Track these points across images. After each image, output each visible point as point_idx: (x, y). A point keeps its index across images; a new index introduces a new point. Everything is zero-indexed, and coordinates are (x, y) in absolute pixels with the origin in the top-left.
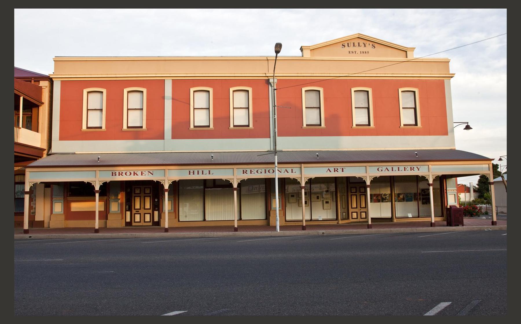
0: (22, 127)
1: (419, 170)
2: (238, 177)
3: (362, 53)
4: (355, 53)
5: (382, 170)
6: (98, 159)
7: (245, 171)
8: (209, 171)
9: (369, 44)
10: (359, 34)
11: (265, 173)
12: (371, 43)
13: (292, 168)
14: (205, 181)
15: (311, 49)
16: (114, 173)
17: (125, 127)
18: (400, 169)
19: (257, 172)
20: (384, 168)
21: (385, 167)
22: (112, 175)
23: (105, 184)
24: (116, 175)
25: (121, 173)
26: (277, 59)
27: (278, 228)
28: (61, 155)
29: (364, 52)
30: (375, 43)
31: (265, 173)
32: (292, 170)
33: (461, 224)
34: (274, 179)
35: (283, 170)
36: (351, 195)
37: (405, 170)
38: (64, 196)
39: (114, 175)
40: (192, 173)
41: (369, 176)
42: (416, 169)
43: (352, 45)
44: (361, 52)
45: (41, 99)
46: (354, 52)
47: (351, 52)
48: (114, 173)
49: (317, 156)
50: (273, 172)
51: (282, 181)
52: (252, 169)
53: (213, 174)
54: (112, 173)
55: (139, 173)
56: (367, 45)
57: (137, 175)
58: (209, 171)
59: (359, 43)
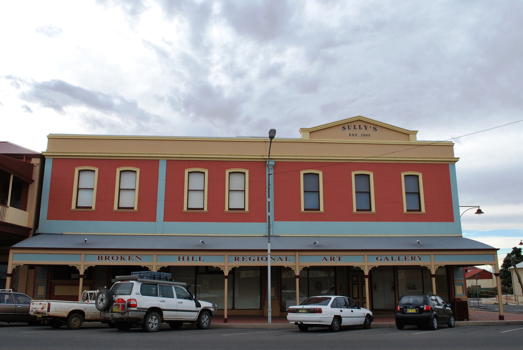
0: (10, 206)
1: (420, 260)
2: (370, 264)
3: (363, 135)
4: (356, 136)
5: (381, 260)
6: (85, 242)
7: (413, 258)
8: (200, 258)
9: (370, 127)
10: (359, 116)
11: (258, 260)
12: (372, 126)
13: (193, 256)
14: (197, 267)
15: (310, 131)
16: (100, 257)
17: (227, 209)
18: (400, 258)
19: (250, 259)
20: (383, 257)
21: (385, 256)
22: (99, 259)
23: (90, 268)
24: (102, 259)
25: (333, 258)
26: (272, 141)
27: (270, 319)
28: (318, 238)
29: (365, 135)
30: (376, 126)
31: (258, 260)
32: (392, 258)
33: (465, 318)
34: (267, 267)
35: (277, 258)
36: (353, 284)
37: (405, 260)
38: (47, 282)
39: (100, 259)
40: (181, 259)
41: (368, 266)
42: (417, 258)
43: (353, 127)
44: (362, 134)
45: (32, 177)
46: (355, 135)
47: (352, 135)
48: (100, 257)
49: (418, 243)
50: (266, 260)
51: (277, 270)
52: (407, 256)
53: (203, 261)
54: (99, 257)
55: (127, 258)
56: (368, 128)
57: (124, 260)
58: (200, 258)
59: (360, 126)
